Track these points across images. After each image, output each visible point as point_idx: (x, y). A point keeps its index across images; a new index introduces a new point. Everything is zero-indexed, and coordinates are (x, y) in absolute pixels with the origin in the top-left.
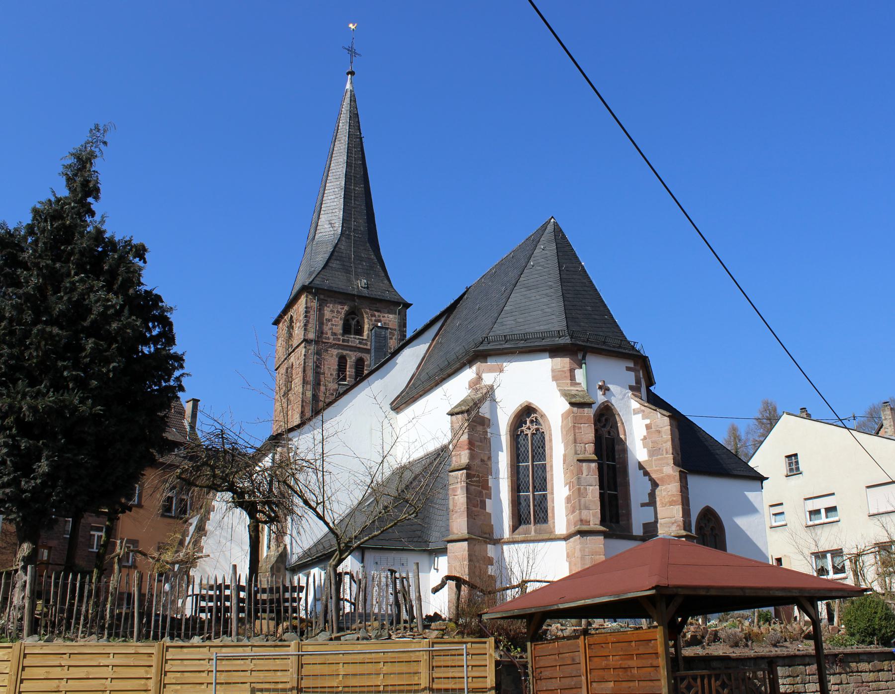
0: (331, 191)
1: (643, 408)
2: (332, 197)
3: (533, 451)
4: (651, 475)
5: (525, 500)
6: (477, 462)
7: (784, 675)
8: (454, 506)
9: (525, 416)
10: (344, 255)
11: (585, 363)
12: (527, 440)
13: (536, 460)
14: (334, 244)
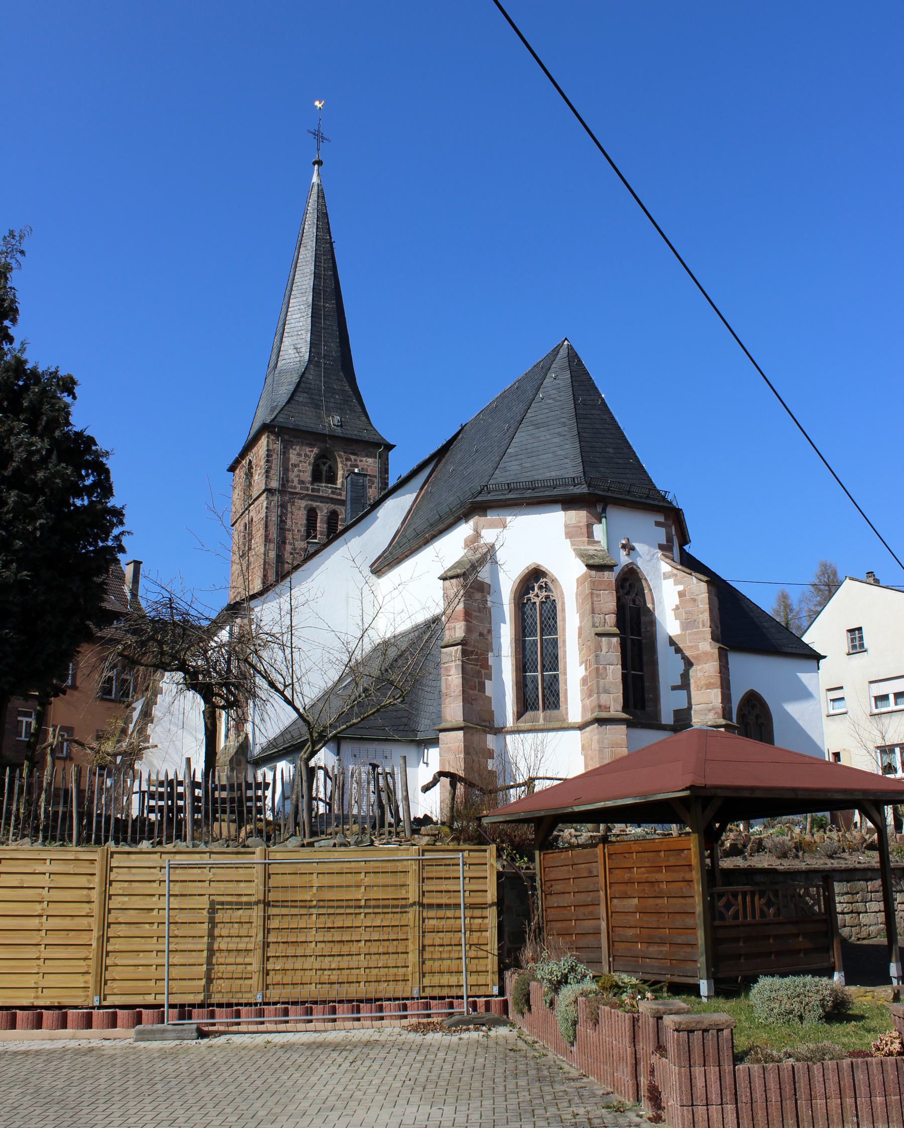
0: (296, 308)
1: (675, 571)
2: (297, 316)
3: (542, 622)
4: (684, 652)
5: (533, 681)
6: (475, 636)
7: (842, 892)
8: (447, 689)
9: (532, 581)
10: (312, 387)
11: (605, 517)
12: (535, 609)
13: (546, 633)
14: (300, 373)
